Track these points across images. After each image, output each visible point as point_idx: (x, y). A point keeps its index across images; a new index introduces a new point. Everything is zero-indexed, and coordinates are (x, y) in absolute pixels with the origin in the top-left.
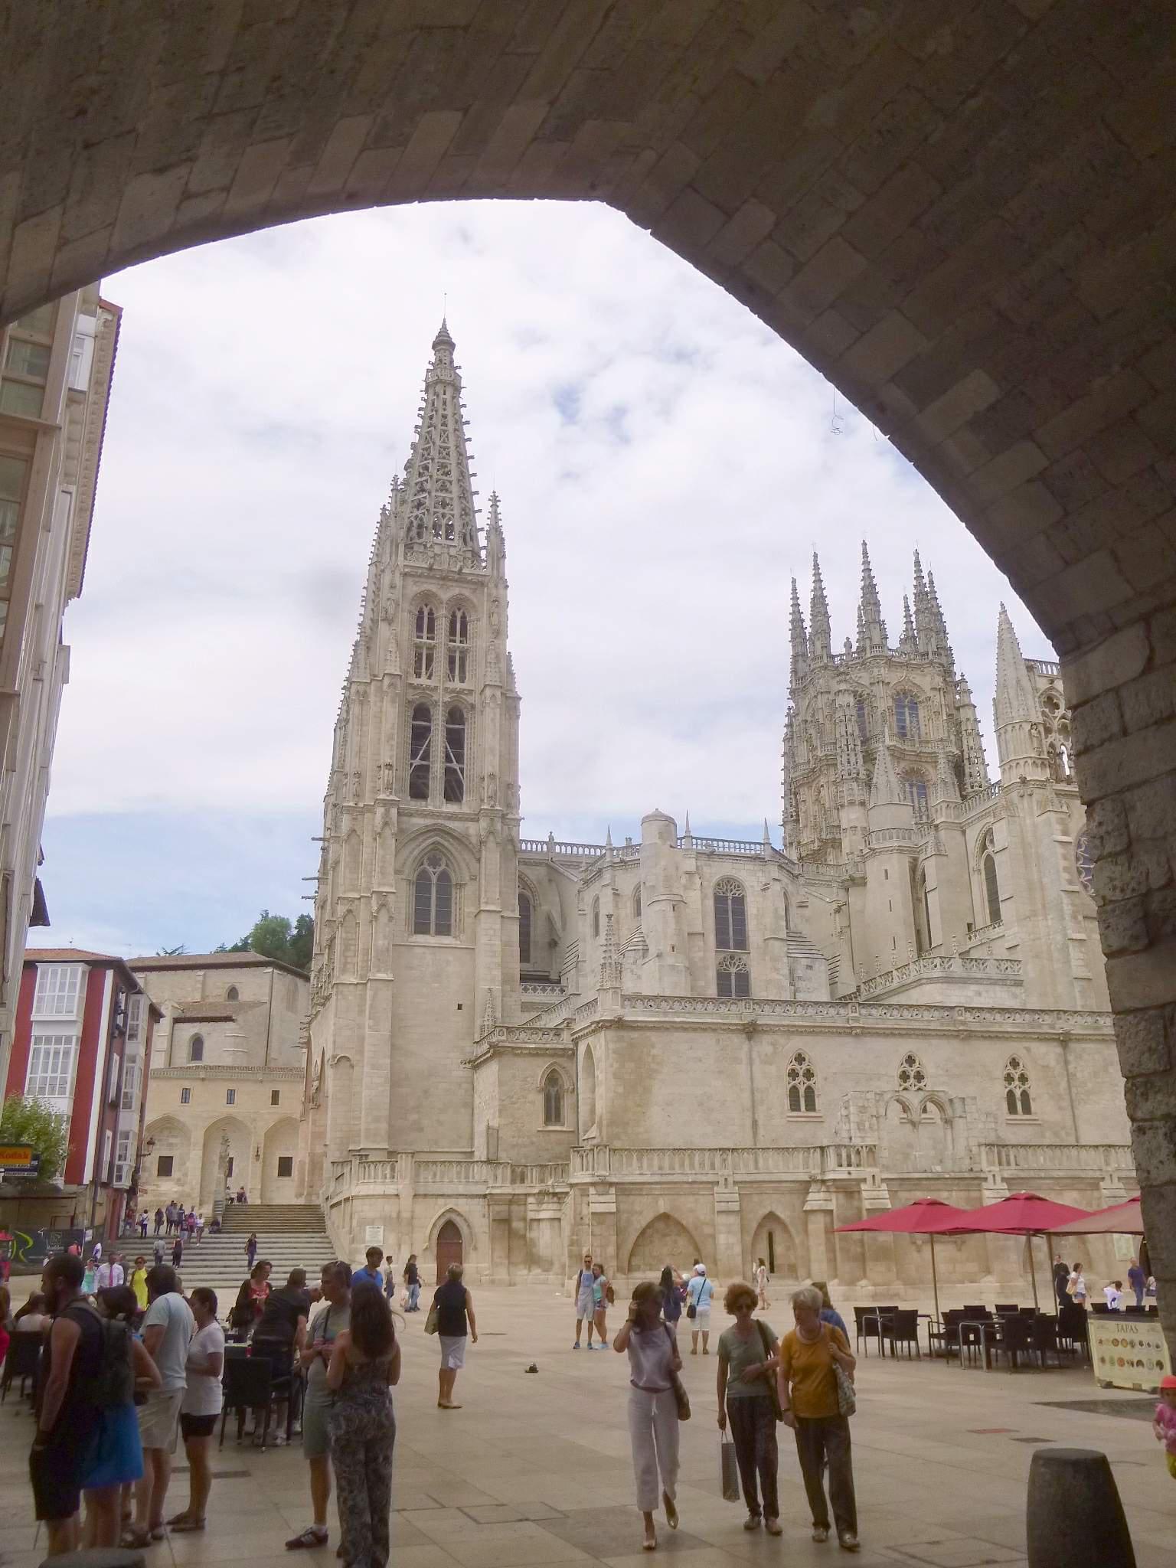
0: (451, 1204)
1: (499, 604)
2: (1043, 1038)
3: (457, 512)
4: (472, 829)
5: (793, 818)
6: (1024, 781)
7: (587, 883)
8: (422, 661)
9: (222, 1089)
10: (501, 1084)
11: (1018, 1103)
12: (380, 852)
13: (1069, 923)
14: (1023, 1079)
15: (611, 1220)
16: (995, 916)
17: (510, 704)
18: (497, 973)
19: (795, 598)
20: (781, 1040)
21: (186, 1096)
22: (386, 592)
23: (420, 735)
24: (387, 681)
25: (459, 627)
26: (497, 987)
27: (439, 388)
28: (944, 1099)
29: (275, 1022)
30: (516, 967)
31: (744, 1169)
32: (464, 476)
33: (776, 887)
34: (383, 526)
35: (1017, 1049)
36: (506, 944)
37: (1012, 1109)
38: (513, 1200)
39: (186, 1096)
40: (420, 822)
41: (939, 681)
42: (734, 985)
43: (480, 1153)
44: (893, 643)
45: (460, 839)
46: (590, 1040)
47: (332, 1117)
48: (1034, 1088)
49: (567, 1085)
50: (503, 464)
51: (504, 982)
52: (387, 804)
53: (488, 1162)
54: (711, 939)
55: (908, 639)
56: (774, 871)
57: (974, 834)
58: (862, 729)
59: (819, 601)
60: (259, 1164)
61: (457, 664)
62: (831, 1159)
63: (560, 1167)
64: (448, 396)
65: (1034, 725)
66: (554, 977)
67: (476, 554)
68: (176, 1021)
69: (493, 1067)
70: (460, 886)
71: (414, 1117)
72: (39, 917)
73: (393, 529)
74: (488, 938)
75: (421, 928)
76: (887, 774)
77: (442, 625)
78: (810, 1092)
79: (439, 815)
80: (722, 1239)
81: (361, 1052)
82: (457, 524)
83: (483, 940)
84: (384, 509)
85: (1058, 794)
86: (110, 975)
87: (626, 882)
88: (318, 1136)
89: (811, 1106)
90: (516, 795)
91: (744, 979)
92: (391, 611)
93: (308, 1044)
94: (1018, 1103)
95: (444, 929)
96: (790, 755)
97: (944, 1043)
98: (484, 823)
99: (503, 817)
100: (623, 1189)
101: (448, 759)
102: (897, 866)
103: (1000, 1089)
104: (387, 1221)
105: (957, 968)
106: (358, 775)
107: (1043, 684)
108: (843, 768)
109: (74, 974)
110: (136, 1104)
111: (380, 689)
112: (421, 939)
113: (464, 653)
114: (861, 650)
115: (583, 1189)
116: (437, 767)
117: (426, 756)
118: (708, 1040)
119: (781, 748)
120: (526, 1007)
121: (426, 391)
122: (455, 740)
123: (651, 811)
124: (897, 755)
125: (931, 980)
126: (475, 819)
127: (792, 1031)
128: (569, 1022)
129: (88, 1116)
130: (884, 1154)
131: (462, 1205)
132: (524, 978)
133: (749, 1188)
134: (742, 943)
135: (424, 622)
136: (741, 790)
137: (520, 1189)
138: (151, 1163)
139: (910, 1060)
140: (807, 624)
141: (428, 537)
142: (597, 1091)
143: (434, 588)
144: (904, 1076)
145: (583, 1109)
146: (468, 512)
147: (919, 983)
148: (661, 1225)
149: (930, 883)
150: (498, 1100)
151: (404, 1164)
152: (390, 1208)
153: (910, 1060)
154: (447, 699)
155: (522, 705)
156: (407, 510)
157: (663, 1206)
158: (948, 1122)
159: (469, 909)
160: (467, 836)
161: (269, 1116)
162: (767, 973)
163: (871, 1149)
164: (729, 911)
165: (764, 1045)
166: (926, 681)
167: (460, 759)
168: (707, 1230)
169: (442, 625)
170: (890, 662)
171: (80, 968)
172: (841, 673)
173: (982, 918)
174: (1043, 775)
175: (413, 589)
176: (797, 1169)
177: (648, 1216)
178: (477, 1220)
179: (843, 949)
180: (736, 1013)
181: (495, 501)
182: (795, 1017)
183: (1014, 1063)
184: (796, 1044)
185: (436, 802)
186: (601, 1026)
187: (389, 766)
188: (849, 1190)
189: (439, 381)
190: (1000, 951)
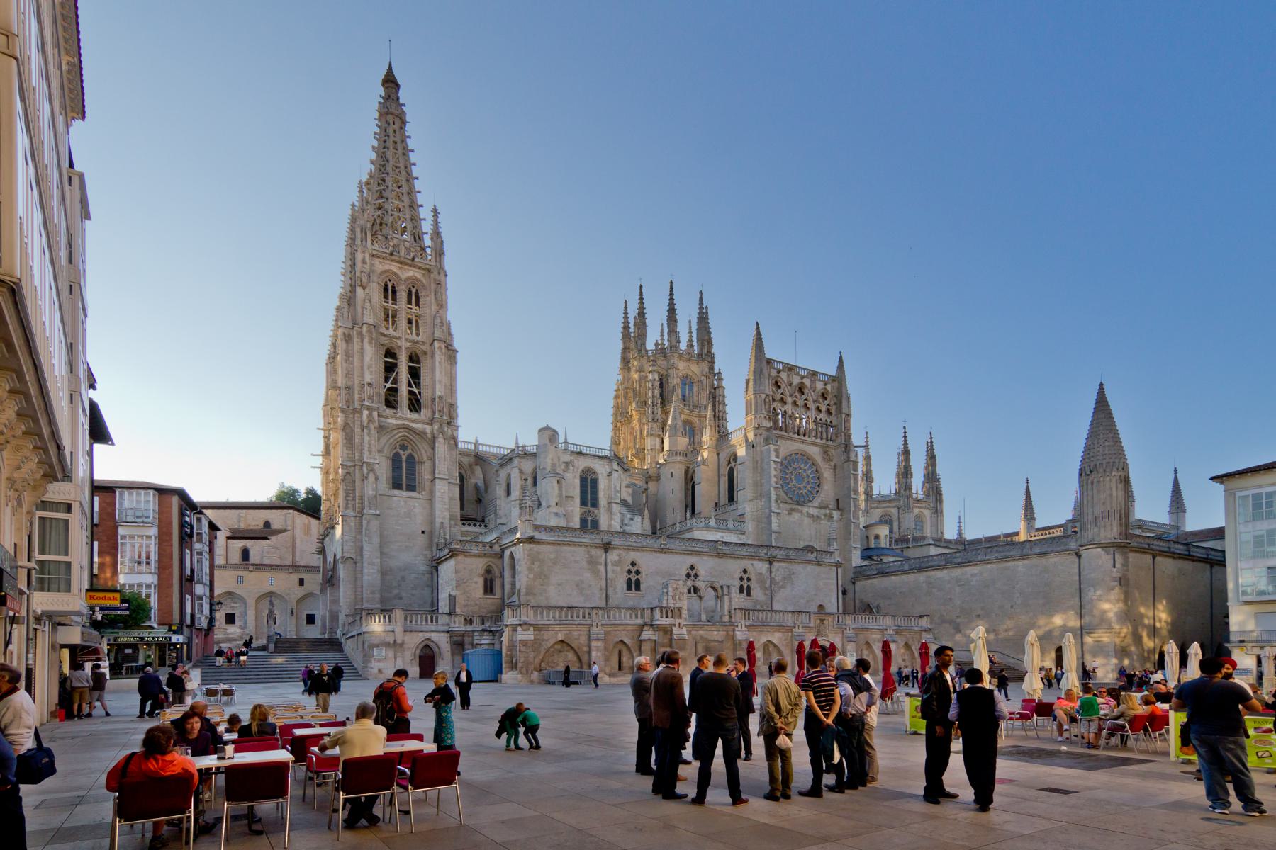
0: (427, 635)
4: (428, 429)
7: (501, 465)
8: (390, 316)
10: (457, 572)
12: (367, 438)
17: (451, 354)
18: (447, 514)
19: (626, 313)
20: (623, 553)
22: (359, 266)
23: (390, 368)
24: (365, 327)
25: (414, 297)
26: (447, 522)
27: (390, 118)
28: (717, 586)
29: (298, 541)
32: (411, 192)
34: (354, 219)
36: (451, 499)
38: (464, 634)
39: (240, 580)
41: (706, 370)
42: (590, 524)
45: (422, 434)
46: (512, 549)
48: (753, 584)
49: (497, 573)
52: (370, 409)
54: (578, 500)
56: (615, 466)
59: (641, 314)
60: (294, 618)
64: (397, 126)
65: (767, 396)
66: (479, 518)
67: (423, 249)
68: (228, 538)
70: (422, 463)
71: (396, 591)
72: (99, 433)
73: (360, 222)
74: (446, 495)
75: (397, 486)
77: (402, 296)
81: (362, 556)
83: (438, 494)
84: (353, 205)
86: (175, 500)
89: (638, 588)
90: (455, 411)
91: (595, 524)
92: (365, 281)
100: (538, 628)
101: (410, 386)
106: (348, 388)
110: (206, 579)
112: (397, 492)
116: (403, 390)
117: (395, 381)
121: (379, 120)
122: (415, 374)
123: (544, 425)
125: (698, 529)
131: (434, 637)
134: (595, 504)
137: (469, 628)
138: (220, 616)
139: (692, 568)
145: (507, 587)
146: (416, 220)
148: (558, 647)
151: (399, 615)
153: (692, 568)
154: (408, 344)
155: (458, 355)
156: (370, 209)
160: (426, 434)
161: (300, 592)
164: (589, 485)
165: (613, 556)
167: (418, 385)
169: (402, 296)
173: (724, 499)
181: (435, 212)
186: (520, 541)
187: (370, 385)
188: (667, 631)
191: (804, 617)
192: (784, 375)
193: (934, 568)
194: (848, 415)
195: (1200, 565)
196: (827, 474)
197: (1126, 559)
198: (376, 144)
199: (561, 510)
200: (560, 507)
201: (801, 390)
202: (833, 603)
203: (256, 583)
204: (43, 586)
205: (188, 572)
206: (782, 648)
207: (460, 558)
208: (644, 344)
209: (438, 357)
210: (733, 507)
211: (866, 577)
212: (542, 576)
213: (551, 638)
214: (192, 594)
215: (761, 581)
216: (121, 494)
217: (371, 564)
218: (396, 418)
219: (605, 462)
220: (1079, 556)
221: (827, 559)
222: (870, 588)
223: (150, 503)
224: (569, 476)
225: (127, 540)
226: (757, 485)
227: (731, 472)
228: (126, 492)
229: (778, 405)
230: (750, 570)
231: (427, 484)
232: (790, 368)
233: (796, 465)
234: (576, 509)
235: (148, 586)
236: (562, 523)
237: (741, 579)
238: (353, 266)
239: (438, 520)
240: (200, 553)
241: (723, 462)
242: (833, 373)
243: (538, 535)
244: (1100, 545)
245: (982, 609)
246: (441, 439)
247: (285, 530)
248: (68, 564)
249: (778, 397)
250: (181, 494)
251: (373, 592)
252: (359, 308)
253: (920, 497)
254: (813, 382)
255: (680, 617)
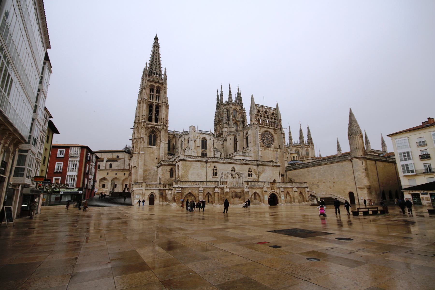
0: (152, 191)
1: (165, 88)
2: (254, 165)
3: (158, 70)
5: (215, 130)
6: (254, 124)
7: (180, 137)
8: (151, 97)
9: (115, 173)
10: (162, 170)
11: (250, 175)
13: (259, 147)
14: (251, 171)
15: (180, 194)
16: (248, 146)
17: (167, 106)
18: (163, 152)
20: (212, 164)
21: (108, 174)
22: (144, 84)
26: (163, 155)
28: (239, 174)
30: (167, 152)
31: (204, 185)
32: (160, 64)
33: (212, 139)
34: (144, 71)
35: (250, 166)
36: (165, 148)
37: (249, 176)
38: (163, 190)
39: (108, 174)
40: (150, 126)
41: (240, 108)
42: (204, 155)
43: (158, 183)
44: (233, 101)
45: (158, 129)
46: (178, 163)
47: (133, 177)
48: (253, 173)
49: (174, 171)
50: (166, 63)
51: (165, 154)
52: (144, 122)
53: (159, 184)
54: (201, 147)
55: (236, 101)
56: (212, 137)
57: (245, 132)
58: (228, 115)
59: (222, 93)
61: (158, 98)
62: (219, 184)
63: (172, 185)
67: (162, 79)
69: (161, 167)
70: (157, 137)
74: (163, 147)
75: (150, 144)
76: (232, 123)
77: (155, 91)
78: (216, 173)
79: (154, 125)
80: (200, 197)
81: (138, 166)
82: (158, 73)
83: (161, 147)
85: (259, 126)
86: (85, 150)
87: (186, 137)
88: (131, 180)
89: (216, 175)
90: (168, 122)
93: (129, 165)
94: (250, 175)
95: (154, 145)
96: (215, 119)
97: (239, 165)
98: (162, 126)
99: (165, 126)
100: (182, 188)
101: (156, 115)
102: (232, 138)
103: (247, 173)
104: (140, 194)
105: (241, 154)
106: (139, 117)
107: (258, 108)
108: (224, 122)
109: (78, 149)
111: (143, 101)
113: (159, 96)
114: (228, 102)
115: (175, 188)
116: (154, 116)
117: (152, 114)
118: (199, 163)
119: (214, 118)
120: (168, 158)
122: (157, 112)
124: (233, 120)
125: (237, 156)
126: (160, 126)
127: (213, 162)
128: (175, 160)
129: (81, 176)
130: (228, 183)
131: (154, 192)
132: (168, 154)
133: (205, 188)
134: (206, 148)
135: (152, 90)
136: (208, 125)
137: (165, 189)
140: (219, 97)
141: (153, 75)
142: (180, 172)
143: (154, 84)
144: (232, 170)
145: (177, 175)
146: (160, 71)
147: (235, 156)
148: (189, 195)
149: (237, 140)
150: (163, 173)
152: (141, 192)
153: (233, 168)
155: (169, 106)
157: (190, 191)
158: (239, 177)
159: (159, 141)
161: (124, 177)
162: (210, 153)
163: (226, 182)
164: (204, 143)
165: (209, 164)
166: (238, 108)
167: (158, 115)
168: (197, 195)
170: (233, 104)
171: (79, 148)
172: (224, 106)
173: (245, 146)
174: (256, 123)
175: (150, 84)
176: (213, 185)
177: (187, 193)
178: (157, 193)
179: (223, 150)
180: (204, 159)
181: (165, 69)
182: (214, 160)
183: (250, 169)
184: (214, 164)
185: (153, 123)
186: (180, 160)
187: (144, 115)
188: (222, 188)
189: (155, 46)
190: (248, 151)
191: (266, 184)
192: (261, 109)
193: (309, 167)
194: (281, 120)
195: (391, 164)
196: (275, 137)
197: (366, 162)
198: (151, 53)
199: (195, 151)
200: (194, 149)
201: (266, 112)
202: (278, 179)
203: (112, 175)
204: (16, 175)
205: (87, 171)
206: (260, 194)
207: (163, 166)
208: (222, 101)
209: (163, 107)
210: (248, 148)
211: (290, 170)
212: (186, 172)
213: (186, 192)
214: (88, 178)
215: (255, 172)
216: (71, 149)
217: (141, 168)
218: (151, 124)
219: (209, 136)
220: (352, 162)
221: (275, 164)
222: (291, 174)
223: (79, 150)
224: (198, 140)
225: (71, 162)
226: (255, 141)
227: (247, 138)
228: (72, 148)
229: (259, 117)
230: (251, 168)
231: (158, 144)
232: (263, 107)
233: (266, 135)
234: (200, 150)
235: (74, 176)
236: (196, 155)
237: (249, 171)
238: (143, 84)
239: (161, 155)
240: (92, 166)
241: (245, 134)
242: (275, 108)
243: (185, 159)
244: (357, 158)
245: (325, 180)
246: (163, 130)
247: (122, 158)
248: (24, 168)
249: (259, 115)
250: (87, 148)
251: (141, 177)
252: (143, 95)
253: (307, 144)
254: (269, 110)
255: (227, 184)
